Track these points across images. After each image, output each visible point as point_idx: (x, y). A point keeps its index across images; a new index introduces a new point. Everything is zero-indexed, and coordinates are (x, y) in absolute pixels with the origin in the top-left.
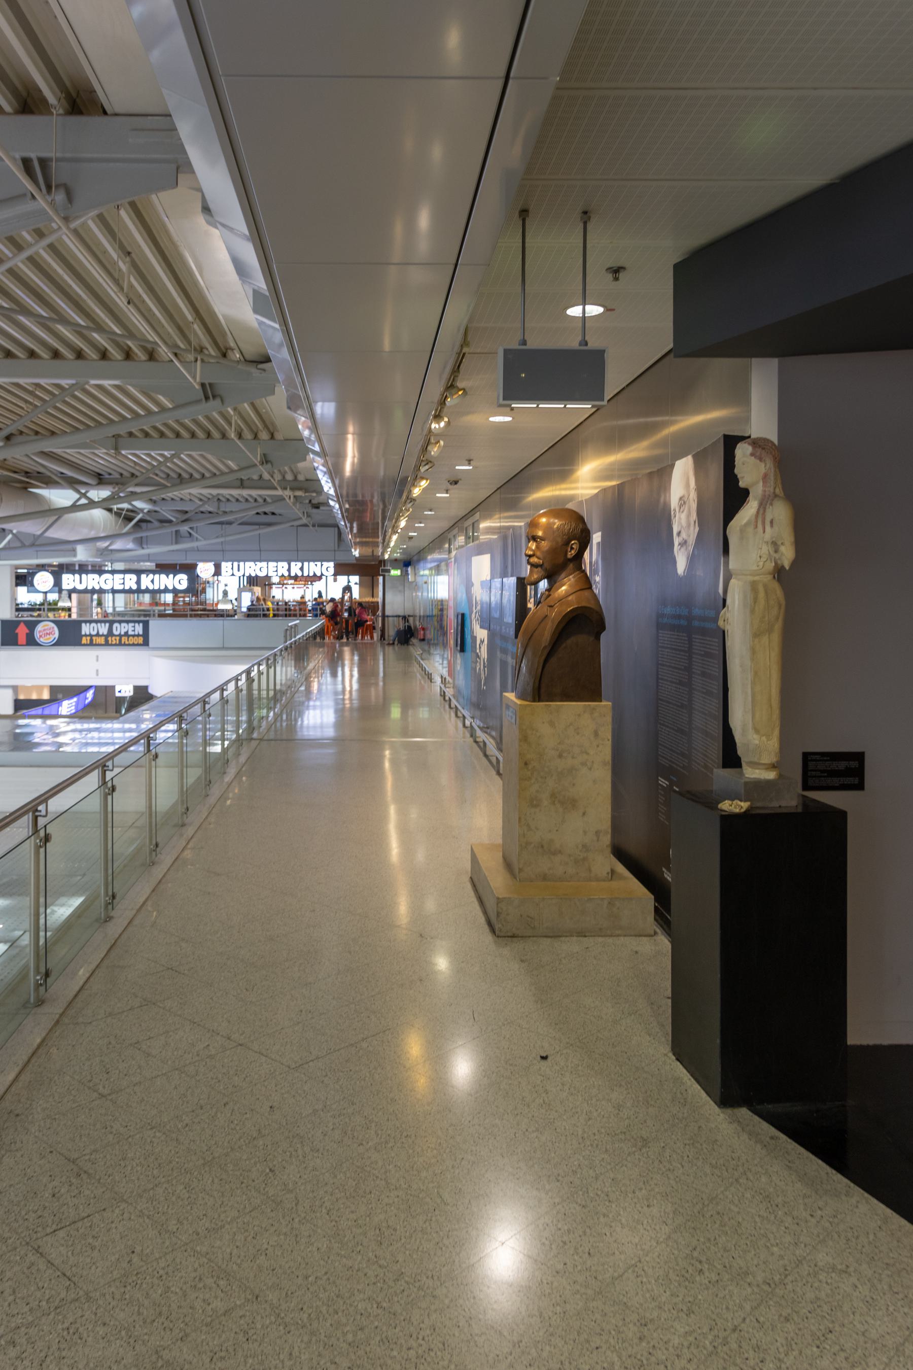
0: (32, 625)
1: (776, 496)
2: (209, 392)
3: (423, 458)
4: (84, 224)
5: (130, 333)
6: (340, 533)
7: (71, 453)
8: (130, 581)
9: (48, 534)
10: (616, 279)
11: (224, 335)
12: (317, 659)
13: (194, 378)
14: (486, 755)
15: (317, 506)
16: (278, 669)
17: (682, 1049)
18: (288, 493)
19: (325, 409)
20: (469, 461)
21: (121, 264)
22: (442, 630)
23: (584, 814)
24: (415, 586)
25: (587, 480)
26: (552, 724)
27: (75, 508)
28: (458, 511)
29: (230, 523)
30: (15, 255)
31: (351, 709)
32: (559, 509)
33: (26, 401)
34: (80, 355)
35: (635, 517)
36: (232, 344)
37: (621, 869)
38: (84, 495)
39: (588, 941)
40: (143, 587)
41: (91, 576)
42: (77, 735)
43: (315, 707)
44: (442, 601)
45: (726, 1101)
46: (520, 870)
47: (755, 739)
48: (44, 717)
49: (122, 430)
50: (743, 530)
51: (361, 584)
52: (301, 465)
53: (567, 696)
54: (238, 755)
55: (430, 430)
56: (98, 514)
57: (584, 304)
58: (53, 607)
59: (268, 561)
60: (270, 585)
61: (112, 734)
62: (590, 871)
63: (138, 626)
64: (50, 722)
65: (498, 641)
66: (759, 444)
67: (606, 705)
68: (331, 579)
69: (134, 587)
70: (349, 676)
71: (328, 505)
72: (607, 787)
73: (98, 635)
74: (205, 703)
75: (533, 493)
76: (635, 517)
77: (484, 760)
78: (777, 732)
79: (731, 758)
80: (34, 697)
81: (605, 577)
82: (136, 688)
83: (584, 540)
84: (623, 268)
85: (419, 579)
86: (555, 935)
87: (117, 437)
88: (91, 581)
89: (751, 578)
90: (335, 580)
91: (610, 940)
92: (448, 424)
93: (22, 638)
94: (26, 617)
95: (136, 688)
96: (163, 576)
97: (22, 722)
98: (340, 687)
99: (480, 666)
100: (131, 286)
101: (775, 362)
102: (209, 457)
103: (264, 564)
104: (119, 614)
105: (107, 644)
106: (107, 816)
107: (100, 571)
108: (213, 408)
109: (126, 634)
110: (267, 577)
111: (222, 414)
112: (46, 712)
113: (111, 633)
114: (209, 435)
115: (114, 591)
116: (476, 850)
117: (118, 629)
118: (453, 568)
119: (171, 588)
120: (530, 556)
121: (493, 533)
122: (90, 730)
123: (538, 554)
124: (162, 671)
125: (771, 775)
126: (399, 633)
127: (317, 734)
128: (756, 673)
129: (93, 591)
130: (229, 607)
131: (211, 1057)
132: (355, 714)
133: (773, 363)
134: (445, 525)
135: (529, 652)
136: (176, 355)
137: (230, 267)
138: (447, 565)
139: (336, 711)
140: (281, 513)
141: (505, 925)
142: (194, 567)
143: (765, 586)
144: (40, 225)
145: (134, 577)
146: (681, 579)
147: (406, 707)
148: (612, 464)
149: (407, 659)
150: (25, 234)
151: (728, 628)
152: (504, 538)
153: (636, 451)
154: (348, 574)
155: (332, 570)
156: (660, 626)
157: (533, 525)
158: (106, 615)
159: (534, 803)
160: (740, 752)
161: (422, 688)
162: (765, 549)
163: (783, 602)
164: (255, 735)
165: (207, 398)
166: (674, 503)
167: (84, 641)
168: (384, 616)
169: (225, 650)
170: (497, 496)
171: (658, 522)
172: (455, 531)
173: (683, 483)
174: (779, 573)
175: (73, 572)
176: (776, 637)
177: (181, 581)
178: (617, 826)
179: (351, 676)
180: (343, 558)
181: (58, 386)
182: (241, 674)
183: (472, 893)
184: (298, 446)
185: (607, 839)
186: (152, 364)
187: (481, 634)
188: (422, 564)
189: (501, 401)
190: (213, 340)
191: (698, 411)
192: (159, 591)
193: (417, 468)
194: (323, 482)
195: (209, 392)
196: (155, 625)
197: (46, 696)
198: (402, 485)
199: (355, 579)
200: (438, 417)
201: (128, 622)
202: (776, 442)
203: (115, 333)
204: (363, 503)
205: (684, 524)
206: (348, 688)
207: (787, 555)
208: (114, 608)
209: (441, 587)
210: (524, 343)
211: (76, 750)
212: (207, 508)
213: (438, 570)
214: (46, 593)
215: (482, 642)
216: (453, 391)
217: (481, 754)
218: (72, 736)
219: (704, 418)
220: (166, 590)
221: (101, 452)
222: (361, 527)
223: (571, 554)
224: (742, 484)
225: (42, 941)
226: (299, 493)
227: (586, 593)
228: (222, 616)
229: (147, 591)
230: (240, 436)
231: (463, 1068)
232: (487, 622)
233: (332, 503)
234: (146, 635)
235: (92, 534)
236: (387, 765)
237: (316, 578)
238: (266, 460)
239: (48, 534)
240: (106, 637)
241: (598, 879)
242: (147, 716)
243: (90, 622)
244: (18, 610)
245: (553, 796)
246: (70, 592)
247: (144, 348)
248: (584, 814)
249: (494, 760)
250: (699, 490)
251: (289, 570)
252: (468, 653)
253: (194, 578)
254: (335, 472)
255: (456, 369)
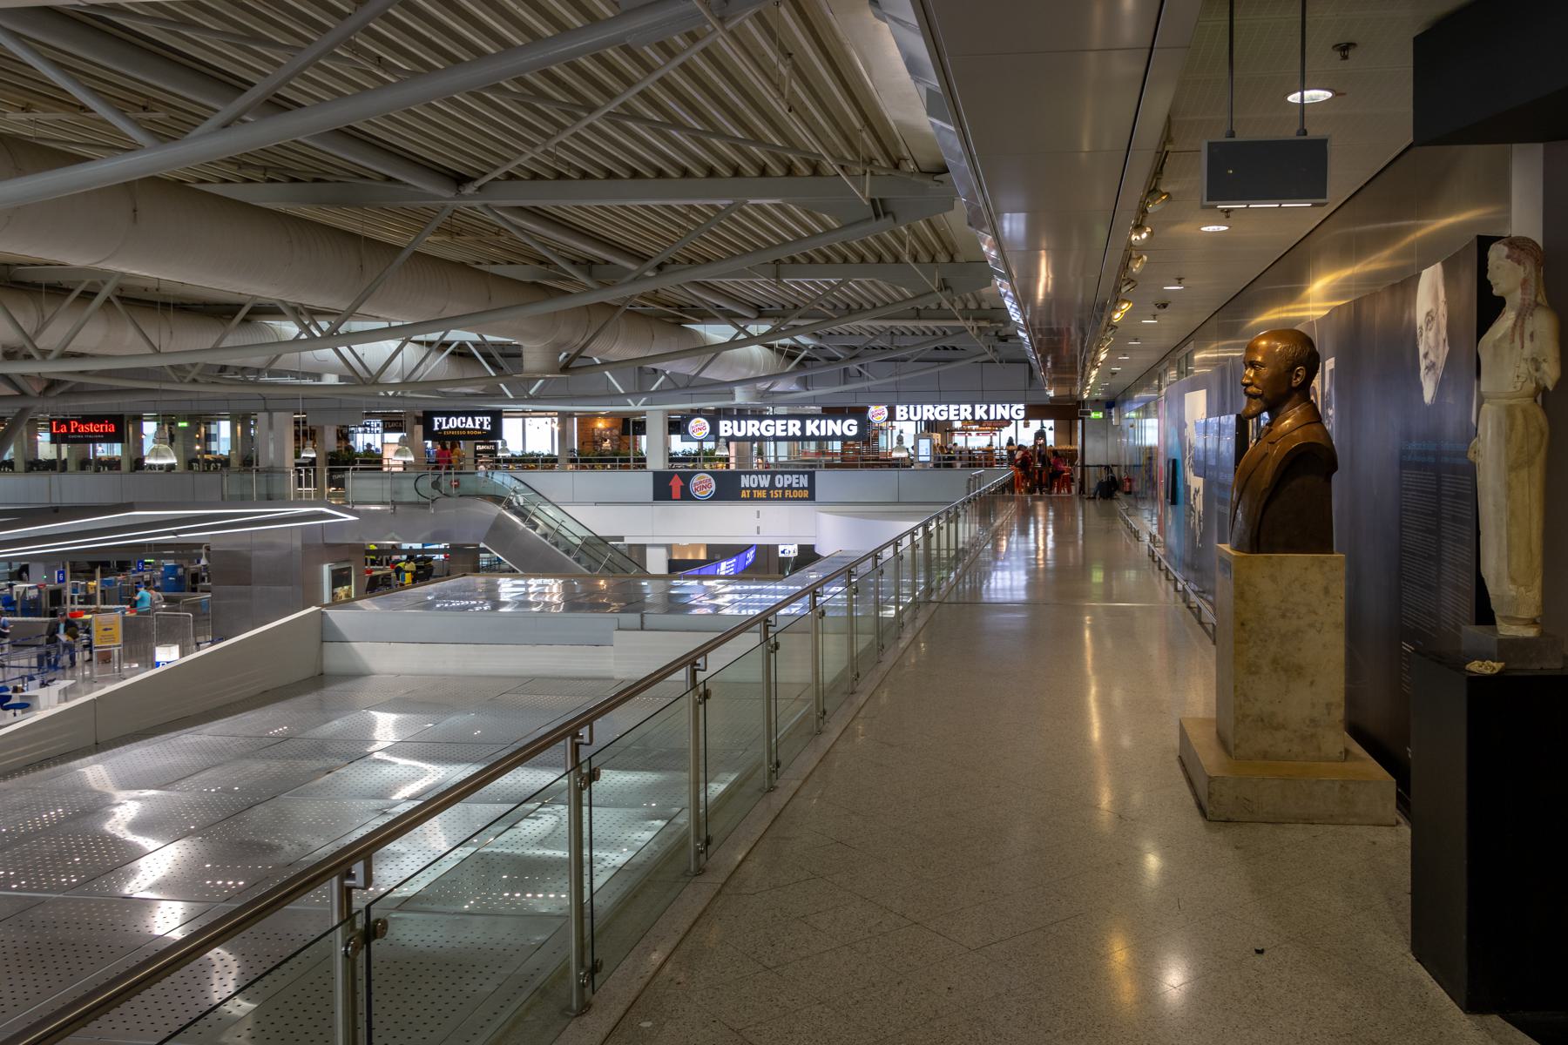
0: (686, 477)
1: (1537, 304)
2: (880, 209)
3: (1124, 274)
4: (741, 24)
5: (792, 146)
6: (1031, 370)
7: (727, 283)
8: (794, 427)
9: (703, 375)
10: (1345, 57)
11: (896, 143)
12: (1007, 514)
13: (863, 193)
14: (1201, 623)
15: (1004, 339)
16: (960, 526)
17: (1423, 950)
18: (970, 323)
19: (1014, 225)
20: (1179, 280)
21: (781, 67)
22: (1152, 482)
23: (1312, 683)
24: (1119, 431)
25: (1318, 298)
26: (1273, 579)
27: (733, 343)
28: (1167, 340)
29: (904, 360)
30: (667, 63)
31: (1046, 570)
32: (1284, 332)
33: (680, 226)
34: (737, 172)
35: (1376, 343)
36: (906, 154)
37: (1357, 749)
38: (743, 330)
39: (1319, 829)
40: (808, 433)
41: (750, 422)
42: (737, 597)
43: (1003, 569)
44: (1151, 448)
45: (1474, 1005)
46: (1236, 746)
47: (1511, 590)
48: (701, 578)
49: (783, 255)
50: (1496, 346)
51: (1057, 430)
52: (985, 291)
53: (1291, 547)
54: (914, 619)
55: (1130, 244)
56: (756, 350)
57: (1302, 90)
58: (709, 457)
59: (948, 403)
60: (952, 431)
61: (772, 592)
62: (1319, 749)
63: (800, 481)
64: (706, 583)
65: (1215, 490)
66: (1518, 246)
67: (1338, 558)
68: (1021, 423)
69: (798, 433)
70: (1042, 537)
71: (1017, 337)
72: (1340, 653)
73: (758, 488)
74: (877, 558)
75: (1253, 316)
76: (1376, 343)
77: (1200, 630)
78: (1538, 582)
79: (1484, 614)
80: (690, 557)
81: (1339, 409)
82: (801, 548)
83: (1311, 362)
84: (1354, 45)
85: (1124, 423)
86: (1277, 821)
87: (777, 262)
88: (751, 427)
89: (1506, 402)
90: (1026, 425)
91: (1343, 829)
92: (1151, 234)
93: (676, 492)
94: (680, 467)
95: (801, 548)
96: (830, 422)
97: (675, 582)
98: (1032, 546)
99: (1194, 520)
100: (793, 92)
101: (1540, 146)
102: (881, 283)
103: (944, 407)
104: (782, 465)
105: (768, 498)
106: (770, 685)
107: (760, 417)
108: (884, 227)
109: (790, 487)
110: (949, 422)
111: (893, 233)
112: (704, 572)
113: (772, 485)
114: (880, 259)
115: (776, 439)
116: (1189, 731)
117: (782, 481)
118: (1163, 410)
119: (839, 433)
120: (1247, 385)
121: (1208, 366)
122: (750, 592)
123: (1257, 382)
124: (830, 530)
125: (1531, 632)
126: (1101, 485)
127: (1000, 597)
128: (1512, 514)
129: (753, 439)
130: (904, 455)
131: (884, 934)
132: (1050, 576)
133: (1538, 149)
134: (1154, 357)
135: (1246, 497)
136: (842, 167)
137: (901, 66)
138: (1157, 405)
139: (1028, 572)
140: (960, 345)
141: (1216, 807)
142: (865, 410)
143: (1524, 411)
144: (694, 28)
145: (798, 423)
146: (1428, 408)
147: (1111, 569)
148: (1348, 279)
149: (1111, 515)
150: (676, 38)
151: (1479, 460)
152: (1223, 370)
153: (1376, 263)
154: (1042, 417)
155: (1022, 414)
156: (1403, 465)
157: (1251, 349)
158: (768, 465)
159: (1253, 670)
160: (1494, 605)
161: (1128, 548)
162: (1524, 368)
163: (1546, 430)
164: (934, 598)
165: (877, 216)
166: (1420, 319)
167: (743, 495)
168: (1083, 466)
169: (899, 504)
170: (1214, 321)
171: (1399, 348)
172: (1166, 364)
173: (1430, 296)
174: (1541, 391)
175: (731, 418)
176: (1537, 471)
177: (850, 427)
178: (1351, 700)
179: (1046, 534)
180: (1035, 399)
181: (713, 207)
182: (917, 528)
183: (1181, 773)
184: (980, 271)
185: (1339, 714)
186: (816, 179)
187: (1196, 483)
188: (1127, 405)
189: (1205, 202)
190: (886, 150)
191: (1449, 212)
192: (827, 438)
193: (1117, 289)
194: (1012, 312)
195: (880, 209)
196: (821, 476)
197: (702, 556)
198: (1102, 309)
199: (1049, 423)
200: (1139, 228)
201: (791, 473)
202: (1540, 244)
203: (775, 145)
204: (1059, 332)
205: (1431, 344)
206: (1041, 547)
207: (1551, 373)
208: (776, 458)
209: (1150, 433)
210: (1232, 134)
211: (735, 612)
212: (879, 343)
213: (1146, 411)
214: (701, 441)
215: (1197, 492)
216: (1156, 195)
217: (1195, 622)
218: (728, 598)
219: (1457, 220)
220: (834, 437)
221: (761, 281)
222: (1051, 363)
223: (1297, 382)
224: (1495, 292)
225: (702, 804)
226: (983, 324)
227: (1315, 428)
228: (897, 466)
229: (813, 438)
230: (915, 260)
231: (1174, 979)
232: (1202, 469)
233: (1021, 334)
234: (811, 488)
235: (752, 374)
236: (1087, 634)
237: (1005, 422)
238: (945, 286)
239: (703, 375)
240: (768, 490)
241: (1328, 760)
242: (812, 575)
243: (750, 473)
244: (671, 460)
245: (1275, 661)
246: (729, 439)
247: (807, 161)
248: (1312, 683)
249: (1210, 628)
250: (1448, 302)
251: (973, 413)
252: (1181, 506)
253: (864, 423)
254: (1025, 297)
255: (1158, 172)
